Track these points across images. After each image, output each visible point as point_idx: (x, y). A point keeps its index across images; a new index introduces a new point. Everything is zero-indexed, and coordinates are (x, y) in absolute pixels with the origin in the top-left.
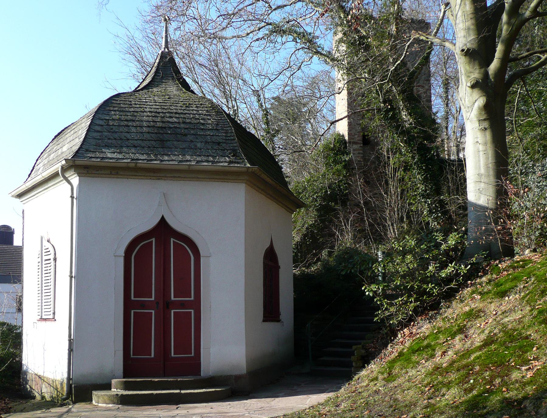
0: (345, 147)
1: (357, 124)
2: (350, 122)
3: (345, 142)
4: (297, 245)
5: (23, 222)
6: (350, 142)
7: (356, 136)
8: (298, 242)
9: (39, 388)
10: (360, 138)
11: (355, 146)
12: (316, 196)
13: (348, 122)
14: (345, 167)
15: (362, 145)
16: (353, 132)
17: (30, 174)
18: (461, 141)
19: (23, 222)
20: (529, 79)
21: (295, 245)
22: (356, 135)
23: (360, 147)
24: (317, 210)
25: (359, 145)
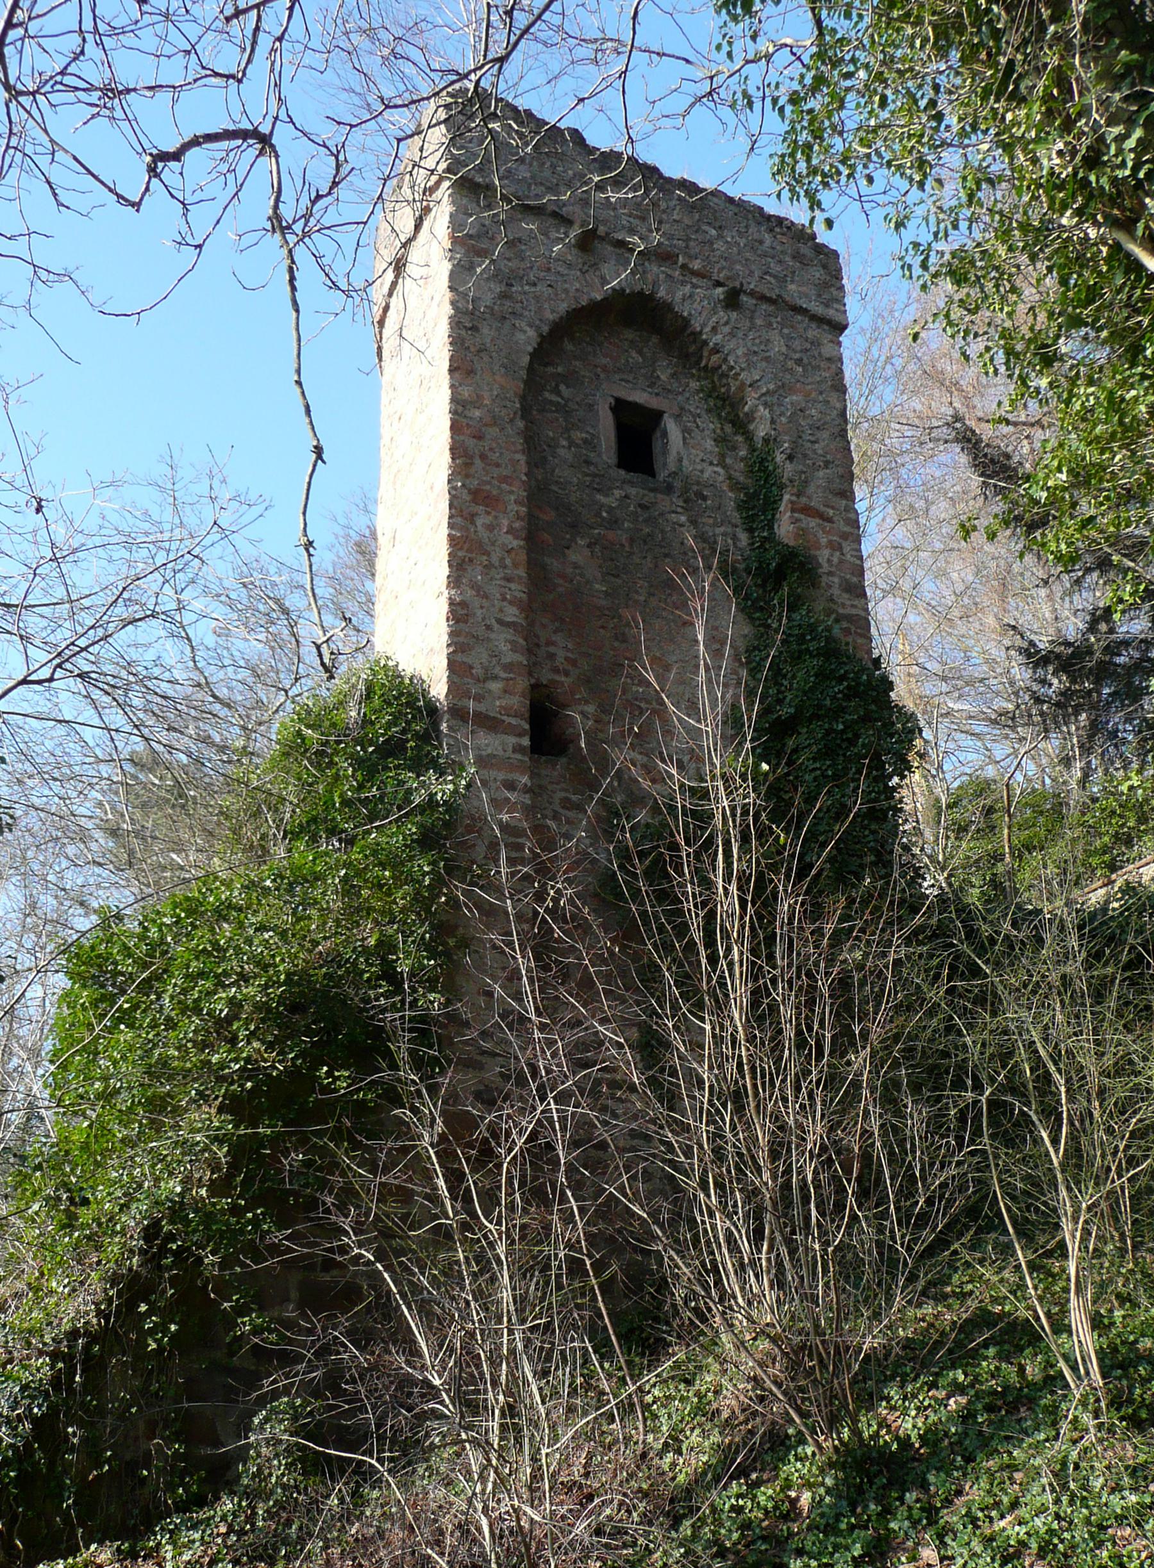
0: (430, 735)
1: (500, 622)
2: (463, 604)
3: (432, 710)
4: (68, 1358)
5: (303, 393)
6: (458, 713)
7: (495, 686)
8: (73, 1334)
9: (831, 512)
10: (517, 701)
11: (490, 742)
12: (231, 1001)
13: (452, 603)
14: (427, 841)
15: (526, 742)
16: (478, 658)
17: (380, 348)
18: (724, 11)
19: (303, 393)
20: (522, 160)
21: (55, 1356)
22: (495, 678)
23: (518, 749)
24: (234, 1106)
25: (512, 740)
